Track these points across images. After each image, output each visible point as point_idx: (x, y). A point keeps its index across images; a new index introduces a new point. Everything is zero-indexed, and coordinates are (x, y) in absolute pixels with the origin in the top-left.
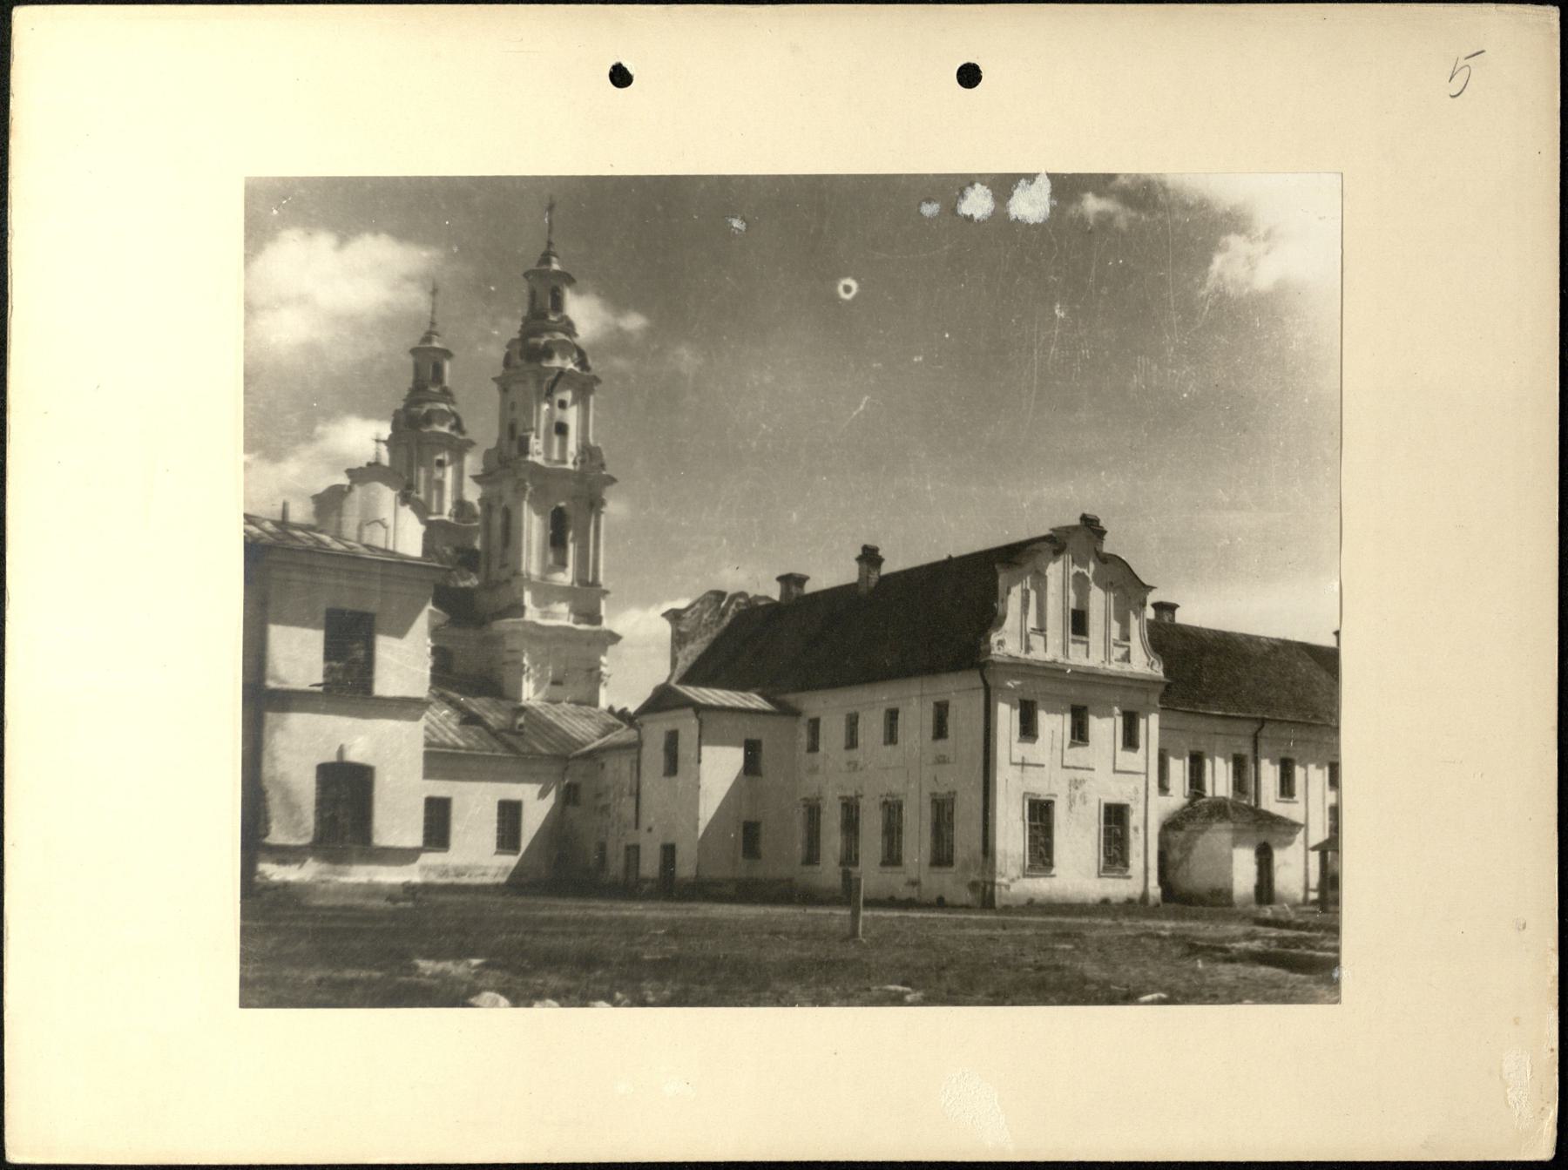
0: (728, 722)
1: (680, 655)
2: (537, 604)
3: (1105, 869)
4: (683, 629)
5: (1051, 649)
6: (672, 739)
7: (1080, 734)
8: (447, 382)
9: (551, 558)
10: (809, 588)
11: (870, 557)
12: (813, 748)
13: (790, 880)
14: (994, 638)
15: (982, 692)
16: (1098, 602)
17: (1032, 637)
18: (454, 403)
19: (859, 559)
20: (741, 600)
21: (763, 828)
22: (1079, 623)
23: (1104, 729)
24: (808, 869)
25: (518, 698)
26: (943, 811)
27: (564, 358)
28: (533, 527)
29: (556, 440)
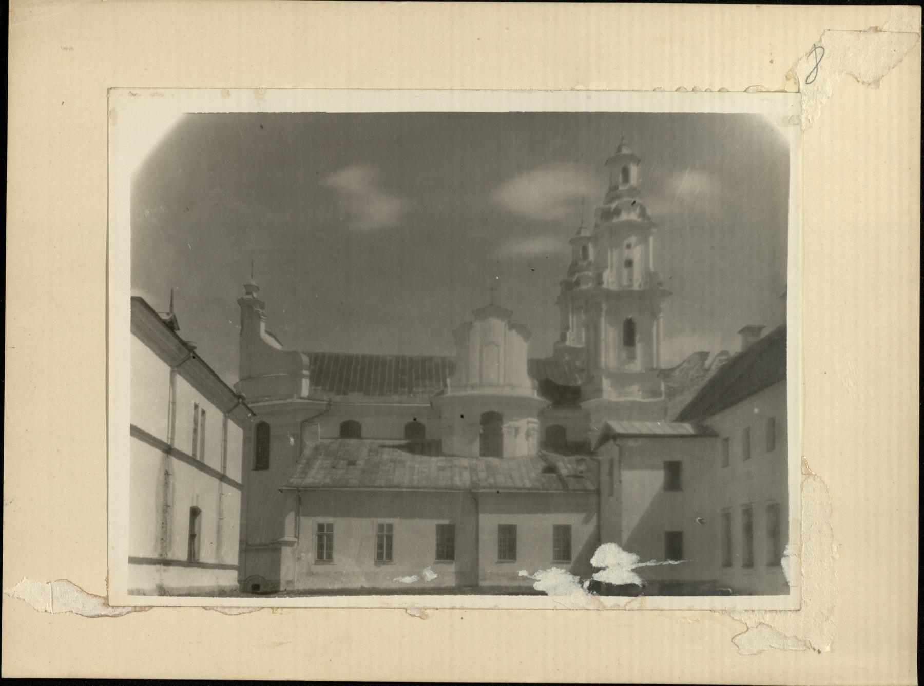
9: (624, 355)
12: (726, 464)
20: (723, 357)
27: (629, 214)
29: (625, 272)
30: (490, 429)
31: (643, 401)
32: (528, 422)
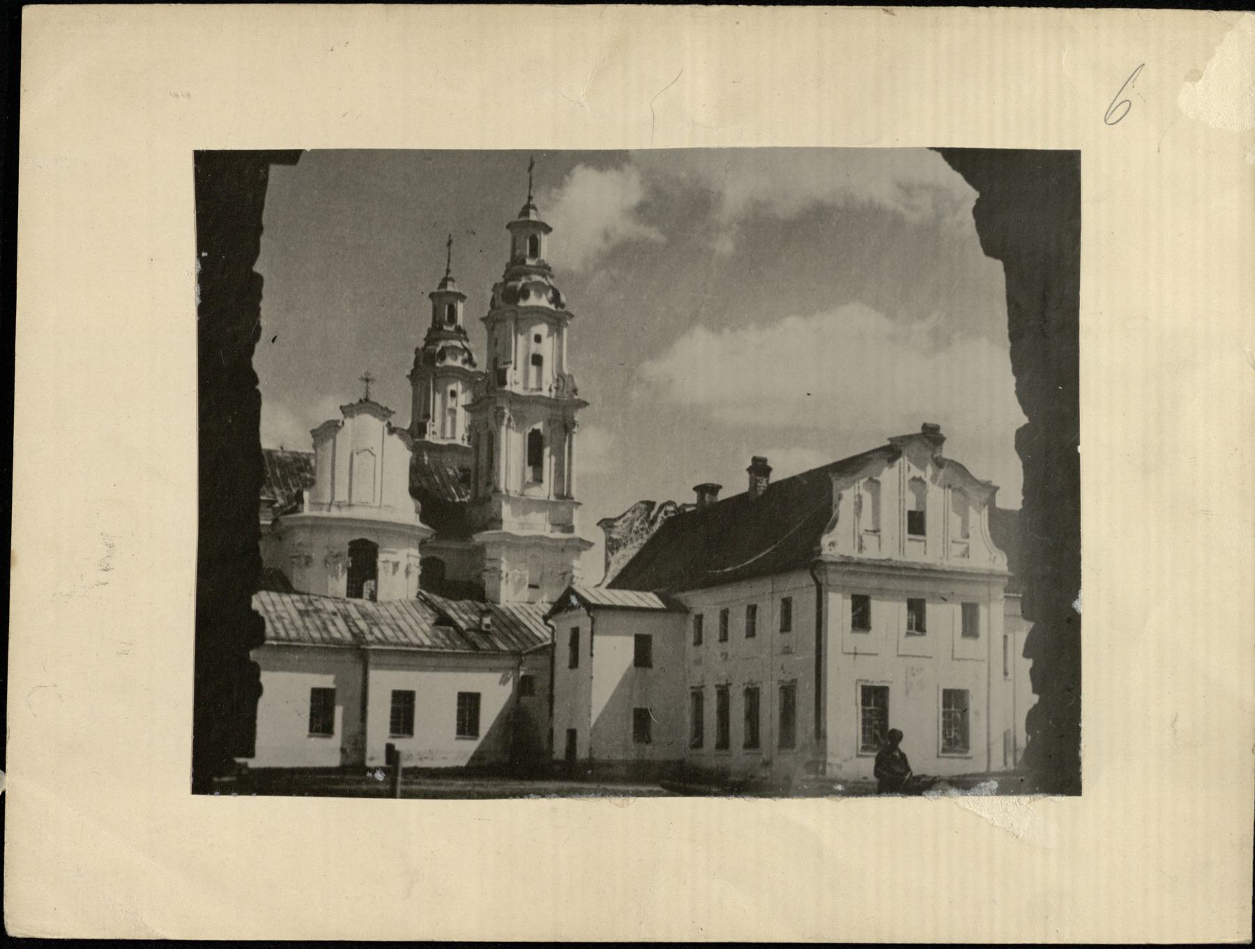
0: (622, 620)
1: (612, 559)
2: (515, 513)
3: (944, 750)
4: (615, 536)
5: (891, 545)
7: (918, 625)
10: (722, 496)
11: (760, 468)
12: (698, 642)
13: (681, 762)
14: (825, 540)
15: (814, 588)
16: (937, 500)
17: (866, 538)
20: (671, 508)
22: (916, 523)
23: (943, 616)
24: (695, 751)
26: (788, 692)
28: (512, 445)
29: (533, 370)
30: (362, 563)
31: (552, 536)
32: (408, 556)
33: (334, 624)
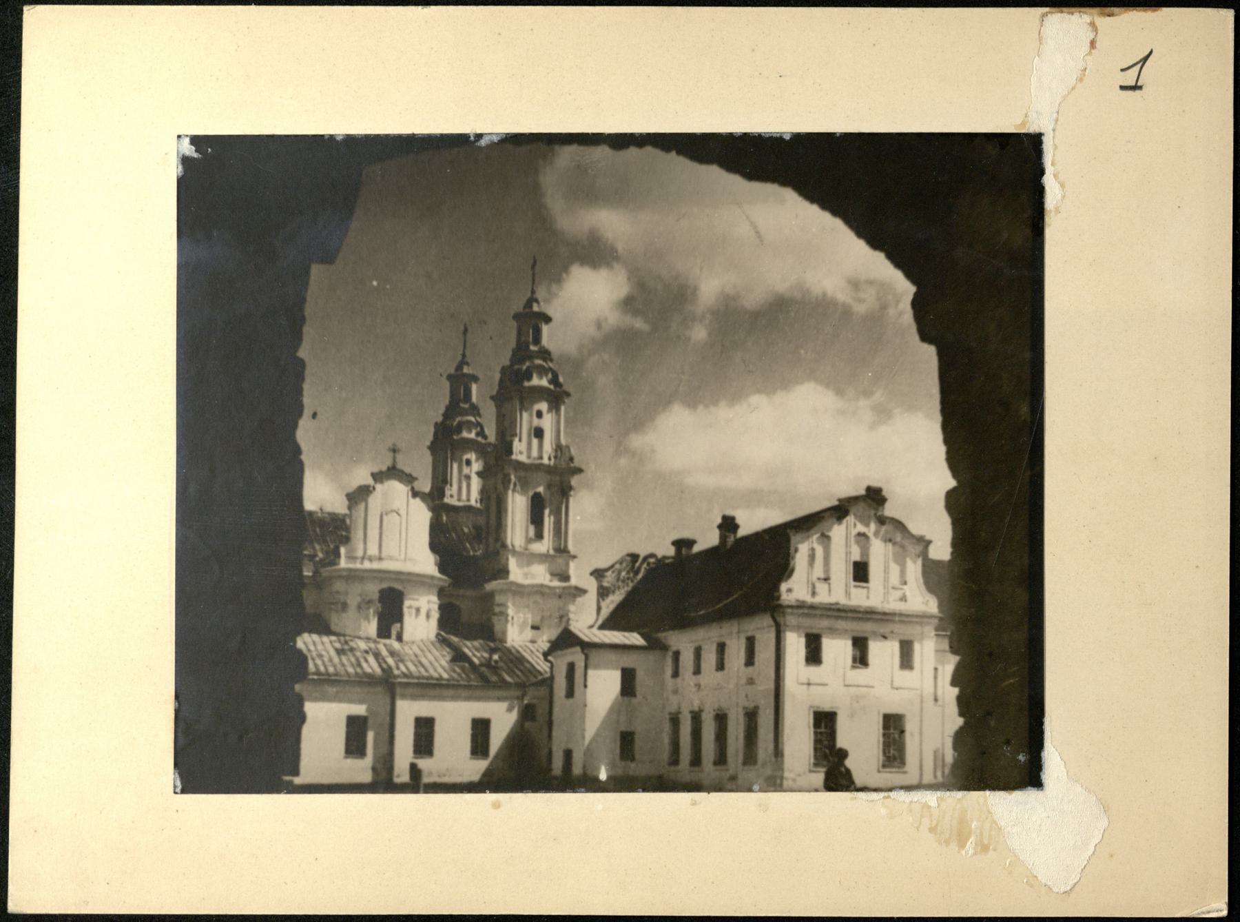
1: (603, 604)
3: (884, 766)
4: (605, 584)
6: (571, 668)
7: (861, 659)
8: (474, 399)
10: (696, 549)
12: (676, 674)
14: (784, 587)
15: (773, 629)
18: (480, 415)
19: (720, 527)
20: (652, 560)
21: (636, 736)
22: (861, 572)
23: (883, 652)
25: (503, 641)
27: (541, 378)
28: (517, 505)
29: (535, 441)
30: (390, 610)
33: (366, 661)
